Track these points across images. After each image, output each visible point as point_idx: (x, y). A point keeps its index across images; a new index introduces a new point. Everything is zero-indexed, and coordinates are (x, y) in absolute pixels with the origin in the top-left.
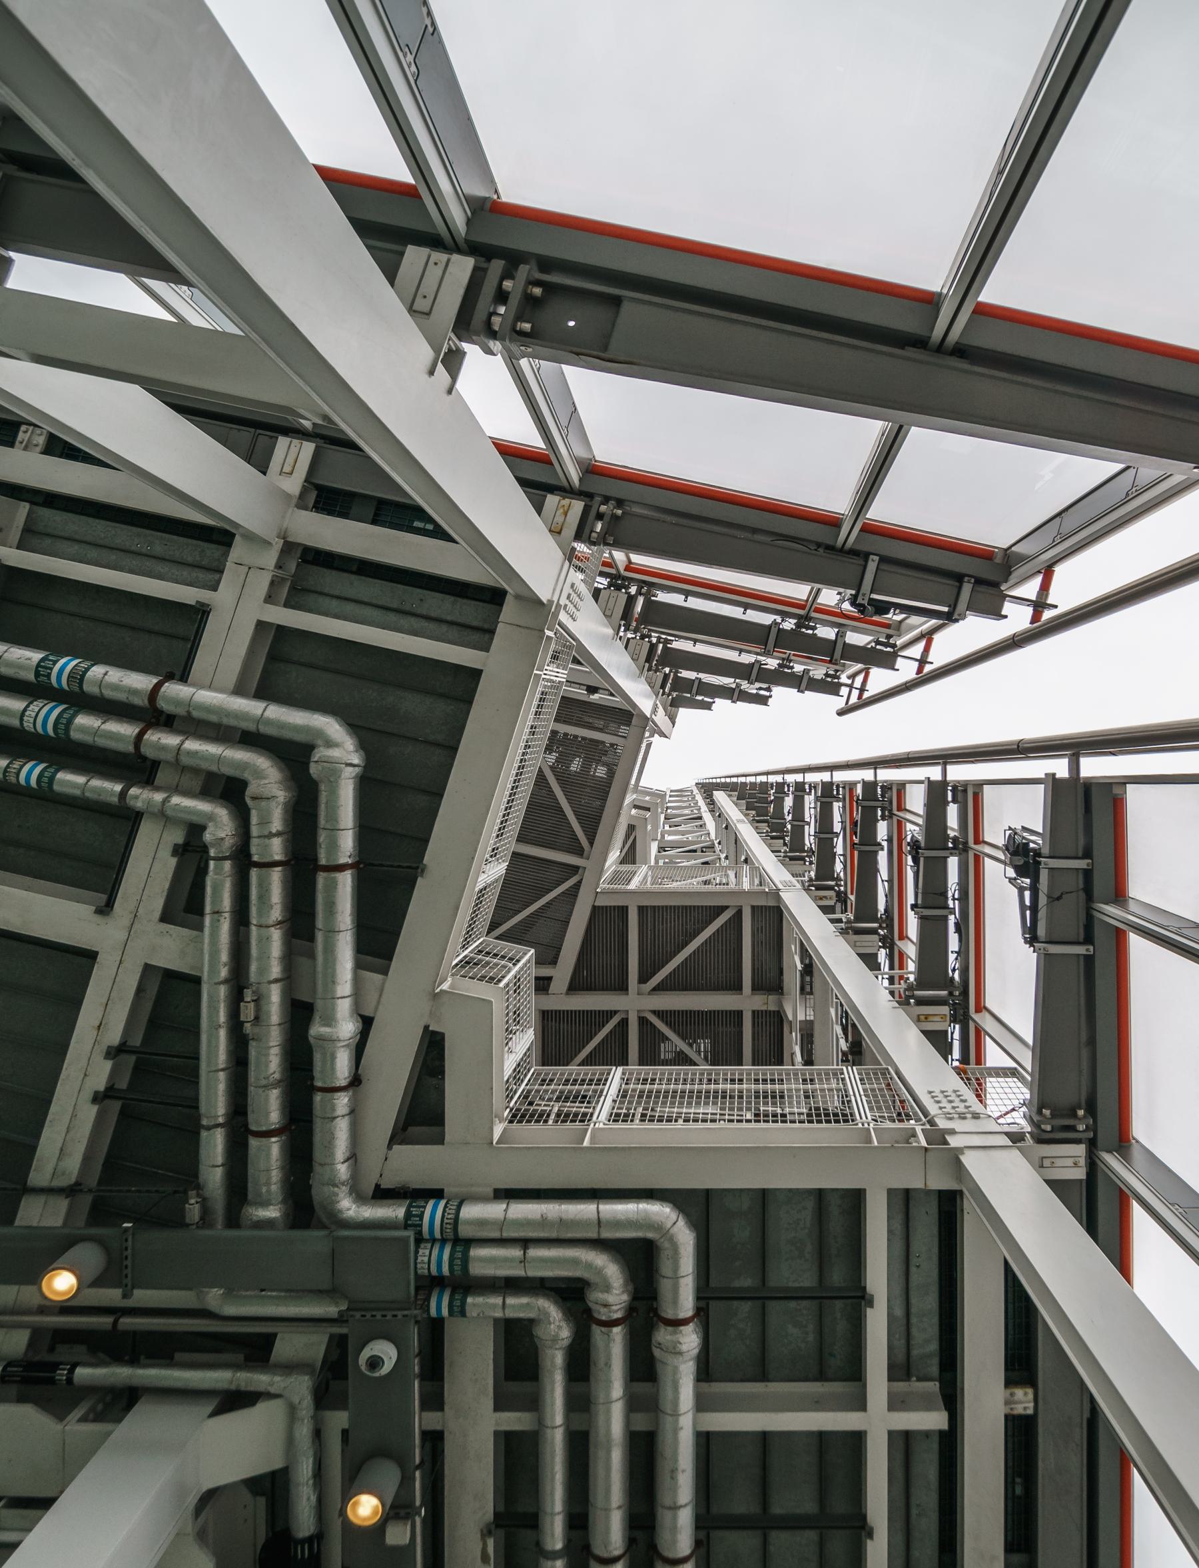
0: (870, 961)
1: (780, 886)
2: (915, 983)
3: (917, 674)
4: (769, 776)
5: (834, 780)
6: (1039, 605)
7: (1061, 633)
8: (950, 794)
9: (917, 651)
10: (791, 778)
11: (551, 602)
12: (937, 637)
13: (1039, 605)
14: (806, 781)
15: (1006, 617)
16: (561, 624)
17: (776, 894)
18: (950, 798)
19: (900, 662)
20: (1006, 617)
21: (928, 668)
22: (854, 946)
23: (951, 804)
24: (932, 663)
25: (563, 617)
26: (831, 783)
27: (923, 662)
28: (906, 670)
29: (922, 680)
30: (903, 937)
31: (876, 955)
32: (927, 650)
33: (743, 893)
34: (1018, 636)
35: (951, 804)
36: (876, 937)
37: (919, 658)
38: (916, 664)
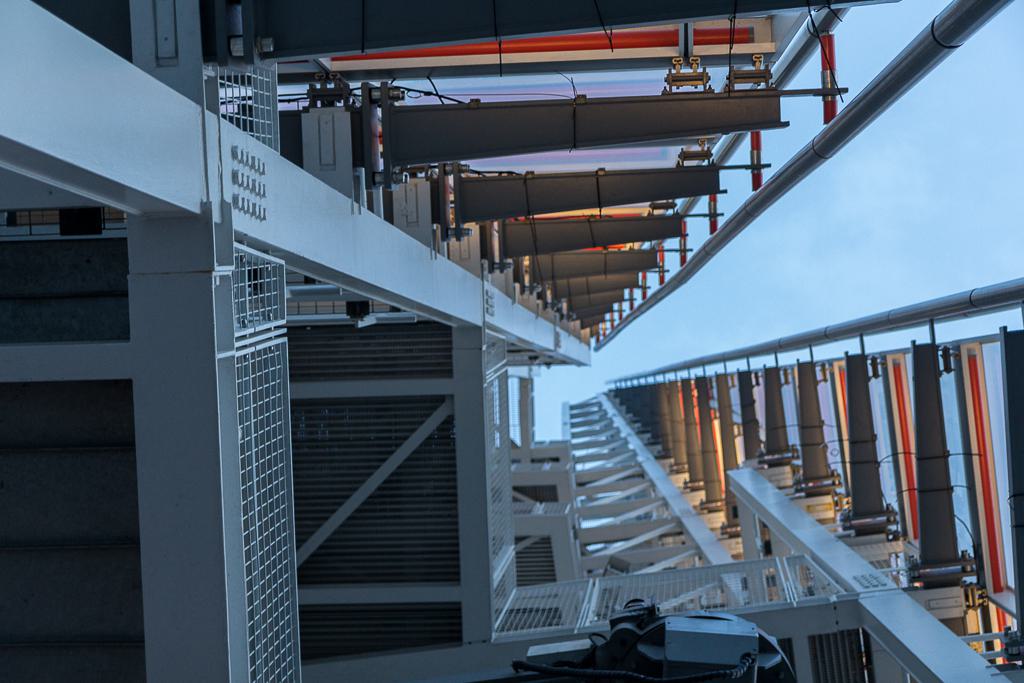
0: (957, 626)
1: (858, 588)
2: (1019, 634)
3: (826, 121)
4: (728, 364)
5: (752, 368)
6: (829, 92)
7: (873, 119)
8: (941, 360)
9: (810, 74)
10: (788, 359)
11: (206, 207)
12: (838, 31)
13: (829, 92)
14: (816, 359)
15: (787, 124)
16: (242, 238)
17: (853, 605)
18: (942, 368)
19: (788, 107)
20: (787, 124)
21: (767, 175)
22: (934, 615)
23: (873, 380)
24: (769, 166)
25: (241, 223)
26: (863, 357)
27: (756, 168)
28: (803, 119)
29: (841, 129)
30: (998, 588)
31: (963, 619)
32: (828, 63)
33: (788, 611)
34: (817, 143)
35: (945, 374)
36: (958, 591)
37: (707, 212)
38: (707, 220)
